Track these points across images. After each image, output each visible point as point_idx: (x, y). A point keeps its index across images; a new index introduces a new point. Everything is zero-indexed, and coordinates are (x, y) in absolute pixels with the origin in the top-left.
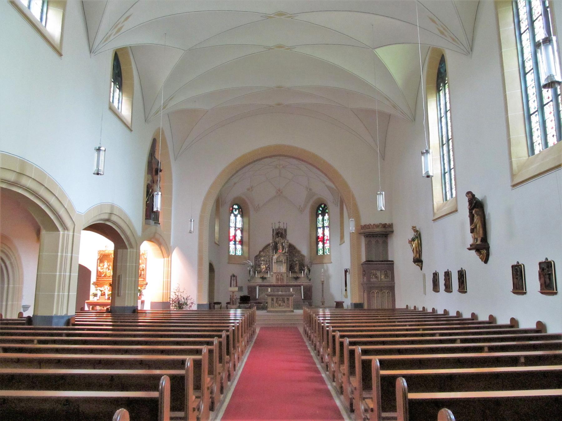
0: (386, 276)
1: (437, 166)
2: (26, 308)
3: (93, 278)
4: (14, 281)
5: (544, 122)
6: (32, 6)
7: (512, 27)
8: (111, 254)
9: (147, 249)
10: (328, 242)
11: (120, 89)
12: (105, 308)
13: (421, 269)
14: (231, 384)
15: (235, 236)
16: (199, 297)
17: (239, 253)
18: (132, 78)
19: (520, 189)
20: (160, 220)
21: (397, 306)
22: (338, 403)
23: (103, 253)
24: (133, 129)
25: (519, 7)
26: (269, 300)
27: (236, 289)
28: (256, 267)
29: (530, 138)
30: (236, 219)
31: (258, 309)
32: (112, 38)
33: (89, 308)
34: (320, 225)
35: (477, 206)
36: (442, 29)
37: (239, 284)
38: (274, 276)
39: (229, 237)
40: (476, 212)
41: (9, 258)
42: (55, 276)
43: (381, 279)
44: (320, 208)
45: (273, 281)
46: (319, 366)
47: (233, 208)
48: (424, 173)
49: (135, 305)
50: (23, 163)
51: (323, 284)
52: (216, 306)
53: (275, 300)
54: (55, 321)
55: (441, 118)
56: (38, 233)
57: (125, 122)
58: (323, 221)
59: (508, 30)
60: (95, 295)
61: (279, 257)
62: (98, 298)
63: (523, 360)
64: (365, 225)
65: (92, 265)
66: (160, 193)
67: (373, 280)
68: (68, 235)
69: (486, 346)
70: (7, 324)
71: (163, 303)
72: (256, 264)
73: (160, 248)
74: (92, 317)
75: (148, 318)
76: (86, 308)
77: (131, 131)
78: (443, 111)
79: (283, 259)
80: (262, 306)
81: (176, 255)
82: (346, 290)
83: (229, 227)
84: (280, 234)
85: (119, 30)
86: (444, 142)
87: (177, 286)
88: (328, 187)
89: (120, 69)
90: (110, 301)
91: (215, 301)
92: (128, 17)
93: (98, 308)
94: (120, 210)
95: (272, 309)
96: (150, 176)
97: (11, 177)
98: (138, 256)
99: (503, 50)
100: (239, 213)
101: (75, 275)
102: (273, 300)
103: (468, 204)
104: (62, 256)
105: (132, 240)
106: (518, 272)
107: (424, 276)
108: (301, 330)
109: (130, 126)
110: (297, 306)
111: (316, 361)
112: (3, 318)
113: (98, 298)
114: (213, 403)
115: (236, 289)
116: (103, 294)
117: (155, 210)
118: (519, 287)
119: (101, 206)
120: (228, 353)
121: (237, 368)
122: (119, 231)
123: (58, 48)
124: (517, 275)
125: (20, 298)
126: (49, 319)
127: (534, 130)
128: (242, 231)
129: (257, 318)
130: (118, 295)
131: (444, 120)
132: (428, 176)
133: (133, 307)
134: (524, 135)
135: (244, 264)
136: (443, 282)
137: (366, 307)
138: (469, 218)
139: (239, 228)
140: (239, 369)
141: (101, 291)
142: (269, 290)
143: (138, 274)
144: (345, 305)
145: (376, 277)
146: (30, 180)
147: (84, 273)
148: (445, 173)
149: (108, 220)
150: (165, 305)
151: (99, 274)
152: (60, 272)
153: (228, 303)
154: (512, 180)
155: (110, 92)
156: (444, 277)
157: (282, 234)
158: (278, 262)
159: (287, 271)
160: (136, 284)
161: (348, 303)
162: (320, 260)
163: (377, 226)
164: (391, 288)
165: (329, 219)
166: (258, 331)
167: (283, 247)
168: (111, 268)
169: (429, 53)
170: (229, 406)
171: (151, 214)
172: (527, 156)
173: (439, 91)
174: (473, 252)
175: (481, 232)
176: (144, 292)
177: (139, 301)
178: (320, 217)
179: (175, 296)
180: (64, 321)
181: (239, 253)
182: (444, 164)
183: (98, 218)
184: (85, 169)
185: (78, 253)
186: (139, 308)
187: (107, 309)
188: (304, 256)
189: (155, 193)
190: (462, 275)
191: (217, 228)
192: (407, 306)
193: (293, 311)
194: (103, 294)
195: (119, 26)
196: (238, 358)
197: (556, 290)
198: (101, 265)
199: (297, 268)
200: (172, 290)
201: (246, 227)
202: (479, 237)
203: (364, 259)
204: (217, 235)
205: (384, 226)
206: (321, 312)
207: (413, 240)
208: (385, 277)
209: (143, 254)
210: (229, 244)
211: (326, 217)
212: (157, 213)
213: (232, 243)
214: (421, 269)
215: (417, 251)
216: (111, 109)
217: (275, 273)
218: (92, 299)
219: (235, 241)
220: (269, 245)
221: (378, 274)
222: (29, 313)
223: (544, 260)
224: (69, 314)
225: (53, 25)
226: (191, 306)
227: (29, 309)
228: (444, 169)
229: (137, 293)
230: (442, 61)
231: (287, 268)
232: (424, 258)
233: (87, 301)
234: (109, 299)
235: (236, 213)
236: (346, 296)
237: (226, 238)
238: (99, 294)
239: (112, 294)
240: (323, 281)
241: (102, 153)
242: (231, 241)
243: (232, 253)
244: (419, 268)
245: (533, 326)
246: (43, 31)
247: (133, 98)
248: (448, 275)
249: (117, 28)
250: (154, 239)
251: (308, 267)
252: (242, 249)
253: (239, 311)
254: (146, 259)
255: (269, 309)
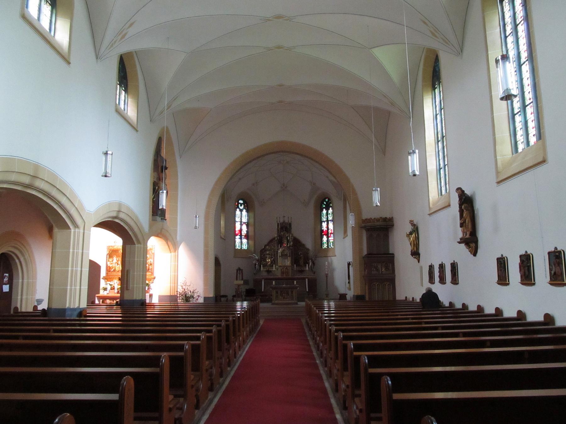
0: (387, 268)
1: (432, 162)
2: (40, 301)
3: (103, 273)
4: (28, 275)
5: (526, 122)
6: (41, 17)
7: (498, 30)
8: (120, 249)
9: (154, 243)
10: (332, 235)
11: (126, 91)
12: (115, 302)
13: (419, 262)
14: (231, 370)
15: (241, 231)
16: (205, 290)
17: (245, 247)
18: (136, 74)
19: (504, 185)
20: (166, 216)
21: (400, 296)
22: (327, 385)
23: (112, 249)
24: (138, 129)
25: (505, 10)
26: (274, 293)
27: (242, 282)
28: (261, 261)
29: (512, 136)
30: (241, 214)
31: (263, 301)
32: (116, 44)
33: (99, 301)
34: (324, 219)
35: (466, 202)
36: (433, 31)
37: (244, 278)
38: (279, 269)
39: (235, 231)
40: (465, 208)
41: (23, 255)
42: (68, 271)
43: (382, 272)
44: (324, 202)
45: (279, 275)
46: (315, 354)
47: (238, 203)
48: (410, 171)
49: (143, 299)
50: (37, 167)
51: (327, 276)
52: (223, 299)
53: (279, 292)
54: (68, 313)
55: (436, 115)
56: (50, 230)
57: (130, 122)
58: (327, 214)
59: (494, 33)
60: (105, 289)
61: (284, 250)
62: (108, 292)
63: (488, 344)
64: (366, 219)
65: (101, 259)
66: (165, 192)
67: (374, 272)
68: (79, 233)
69: (461, 332)
70: (21, 316)
71: (171, 296)
72: (261, 258)
73: (168, 244)
74: (103, 310)
75: (157, 310)
76: (97, 302)
77: (137, 131)
78: (438, 109)
79: (287, 252)
80: (266, 298)
81: (182, 250)
82: (349, 283)
83: (235, 222)
84: (285, 228)
85: (123, 37)
86: (439, 139)
87: (184, 279)
88: (331, 181)
89: (126, 73)
90: (119, 295)
91: (222, 294)
92: (132, 25)
93: (108, 301)
94: (128, 208)
95: (276, 302)
96: (156, 173)
97: (26, 180)
98: (145, 251)
99: (489, 52)
100: (244, 208)
101: (86, 270)
102: (277, 292)
103: (458, 199)
104: (73, 252)
105: (139, 236)
106: (502, 263)
107: (421, 268)
108: (303, 321)
109: (136, 127)
110: (301, 299)
111: (313, 349)
112: (19, 310)
113: (108, 292)
114: (212, 384)
115: (242, 282)
116: (113, 288)
117: (160, 207)
118: (503, 279)
119: (110, 204)
120: (228, 341)
121: (238, 356)
122: (126, 228)
123: (66, 57)
124: (501, 267)
125: (34, 292)
126: (63, 311)
127: (518, 129)
128: (248, 225)
129: (261, 310)
130: (127, 289)
131: (439, 117)
132: (415, 175)
133: (141, 300)
134: (508, 134)
135: (250, 258)
136: (438, 273)
137: (367, 298)
138: (459, 213)
139: (244, 223)
140: (241, 356)
141: (111, 285)
142: (295, 282)
143: (145, 268)
144: (348, 298)
145: (377, 270)
146: (44, 182)
147: (94, 268)
148: (440, 169)
149: (116, 217)
150: (173, 298)
151: (108, 269)
152: (72, 267)
153: (234, 296)
154: (497, 177)
155: (116, 94)
156: (438, 270)
157: (286, 228)
158: (284, 255)
159: (292, 264)
160: (144, 278)
161: (350, 295)
162: (324, 253)
163: (378, 220)
164: (392, 281)
165: (333, 213)
166: (261, 322)
167: (288, 241)
168: (120, 263)
169: (424, 52)
170: (227, 388)
171: (157, 212)
172: (511, 154)
173: (434, 89)
174: (463, 245)
175: (470, 226)
176: (152, 285)
177: (147, 295)
178: (324, 211)
179: (182, 289)
180: (76, 313)
181: (245, 247)
182: (439, 160)
183: (106, 216)
184: (92, 166)
185: (88, 250)
186: (148, 301)
187: (117, 302)
188: (308, 250)
189: (161, 192)
190: (454, 267)
191: (222, 223)
192: (406, 297)
193: (297, 304)
194: (113, 288)
195: (124, 33)
196: (240, 346)
197: (534, 281)
198: (111, 260)
199: (302, 262)
200: (179, 284)
201: (252, 221)
202: (468, 231)
203: (365, 252)
204: (223, 230)
205: (385, 219)
206: (326, 303)
207: (411, 233)
208: (385, 269)
209: (151, 249)
210: (235, 238)
211: (330, 211)
212: (163, 211)
213: (238, 237)
214: (419, 262)
215: (414, 244)
216: (118, 111)
217: (280, 266)
218: (102, 293)
219: (241, 235)
220: (274, 238)
221: (379, 267)
222: (44, 306)
223: (524, 253)
224: (81, 307)
225: (62, 35)
226: (197, 299)
227: (43, 302)
228: (440, 165)
229: (145, 286)
230: (437, 59)
231: (292, 261)
232: (421, 251)
233: (97, 295)
234: (118, 292)
235: (242, 208)
236: (350, 289)
237: (231, 233)
238: (109, 288)
239: (121, 288)
240: (327, 274)
241: (109, 157)
242: (237, 235)
243: (238, 246)
244: (416, 260)
245: (541, 319)
246: (52, 42)
247: (138, 100)
248: (442, 267)
249: (122, 35)
250: (160, 234)
251: (312, 260)
252: (248, 243)
253: (245, 304)
254: (154, 254)
255: (273, 302)
